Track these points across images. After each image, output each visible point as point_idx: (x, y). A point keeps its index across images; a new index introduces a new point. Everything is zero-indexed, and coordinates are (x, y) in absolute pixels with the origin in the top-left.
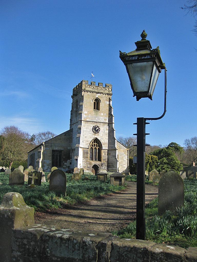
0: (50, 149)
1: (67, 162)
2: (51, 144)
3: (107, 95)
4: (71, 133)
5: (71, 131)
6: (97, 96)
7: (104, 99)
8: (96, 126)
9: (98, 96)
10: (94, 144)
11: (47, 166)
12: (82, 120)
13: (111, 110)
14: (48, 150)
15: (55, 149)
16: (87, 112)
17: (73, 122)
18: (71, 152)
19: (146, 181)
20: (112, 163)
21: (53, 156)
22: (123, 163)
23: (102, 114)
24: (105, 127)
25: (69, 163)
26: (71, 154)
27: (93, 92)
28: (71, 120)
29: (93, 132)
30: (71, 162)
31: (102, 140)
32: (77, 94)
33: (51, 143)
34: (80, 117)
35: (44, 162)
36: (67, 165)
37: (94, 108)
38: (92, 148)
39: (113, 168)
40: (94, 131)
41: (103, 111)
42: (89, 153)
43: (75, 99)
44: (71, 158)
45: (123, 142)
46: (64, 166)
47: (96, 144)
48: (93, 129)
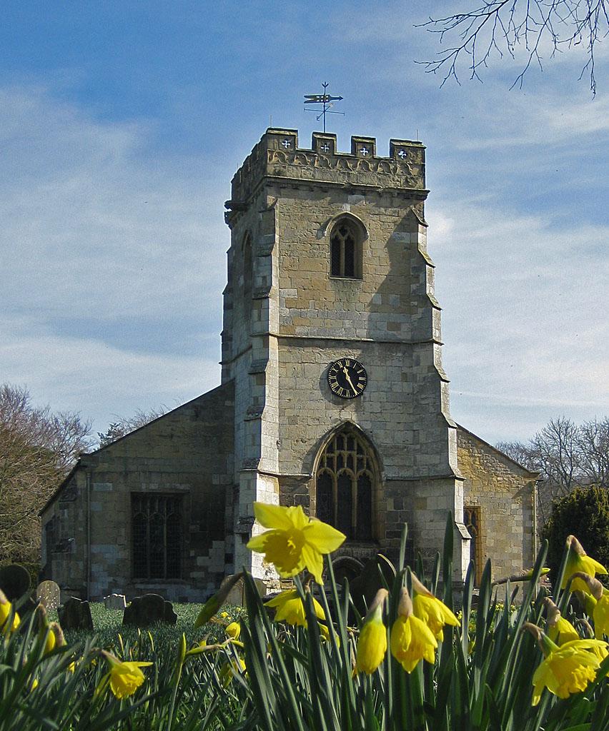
0: (122, 488)
1: (211, 551)
4: (228, 403)
5: (226, 392)
7: (384, 218)
8: (362, 382)
10: (340, 457)
11: (109, 576)
12: (271, 331)
13: (422, 275)
14: (109, 492)
16: (294, 291)
21: (137, 524)
22: (508, 550)
24: (396, 363)
26: (228, 511)
29: (333, 393)
30: (229, 552)
31: (381, 433)
32: (248, 205)
34: (260, 320)
35: (93, 554)
36: (210, 570)
37: (335, 271)
40: (337, 389)
41: (389, 386)
43: (242, 230)
45: (509, 451)
46: (195, 574)
47: (346, 453)
48: (331, 377)
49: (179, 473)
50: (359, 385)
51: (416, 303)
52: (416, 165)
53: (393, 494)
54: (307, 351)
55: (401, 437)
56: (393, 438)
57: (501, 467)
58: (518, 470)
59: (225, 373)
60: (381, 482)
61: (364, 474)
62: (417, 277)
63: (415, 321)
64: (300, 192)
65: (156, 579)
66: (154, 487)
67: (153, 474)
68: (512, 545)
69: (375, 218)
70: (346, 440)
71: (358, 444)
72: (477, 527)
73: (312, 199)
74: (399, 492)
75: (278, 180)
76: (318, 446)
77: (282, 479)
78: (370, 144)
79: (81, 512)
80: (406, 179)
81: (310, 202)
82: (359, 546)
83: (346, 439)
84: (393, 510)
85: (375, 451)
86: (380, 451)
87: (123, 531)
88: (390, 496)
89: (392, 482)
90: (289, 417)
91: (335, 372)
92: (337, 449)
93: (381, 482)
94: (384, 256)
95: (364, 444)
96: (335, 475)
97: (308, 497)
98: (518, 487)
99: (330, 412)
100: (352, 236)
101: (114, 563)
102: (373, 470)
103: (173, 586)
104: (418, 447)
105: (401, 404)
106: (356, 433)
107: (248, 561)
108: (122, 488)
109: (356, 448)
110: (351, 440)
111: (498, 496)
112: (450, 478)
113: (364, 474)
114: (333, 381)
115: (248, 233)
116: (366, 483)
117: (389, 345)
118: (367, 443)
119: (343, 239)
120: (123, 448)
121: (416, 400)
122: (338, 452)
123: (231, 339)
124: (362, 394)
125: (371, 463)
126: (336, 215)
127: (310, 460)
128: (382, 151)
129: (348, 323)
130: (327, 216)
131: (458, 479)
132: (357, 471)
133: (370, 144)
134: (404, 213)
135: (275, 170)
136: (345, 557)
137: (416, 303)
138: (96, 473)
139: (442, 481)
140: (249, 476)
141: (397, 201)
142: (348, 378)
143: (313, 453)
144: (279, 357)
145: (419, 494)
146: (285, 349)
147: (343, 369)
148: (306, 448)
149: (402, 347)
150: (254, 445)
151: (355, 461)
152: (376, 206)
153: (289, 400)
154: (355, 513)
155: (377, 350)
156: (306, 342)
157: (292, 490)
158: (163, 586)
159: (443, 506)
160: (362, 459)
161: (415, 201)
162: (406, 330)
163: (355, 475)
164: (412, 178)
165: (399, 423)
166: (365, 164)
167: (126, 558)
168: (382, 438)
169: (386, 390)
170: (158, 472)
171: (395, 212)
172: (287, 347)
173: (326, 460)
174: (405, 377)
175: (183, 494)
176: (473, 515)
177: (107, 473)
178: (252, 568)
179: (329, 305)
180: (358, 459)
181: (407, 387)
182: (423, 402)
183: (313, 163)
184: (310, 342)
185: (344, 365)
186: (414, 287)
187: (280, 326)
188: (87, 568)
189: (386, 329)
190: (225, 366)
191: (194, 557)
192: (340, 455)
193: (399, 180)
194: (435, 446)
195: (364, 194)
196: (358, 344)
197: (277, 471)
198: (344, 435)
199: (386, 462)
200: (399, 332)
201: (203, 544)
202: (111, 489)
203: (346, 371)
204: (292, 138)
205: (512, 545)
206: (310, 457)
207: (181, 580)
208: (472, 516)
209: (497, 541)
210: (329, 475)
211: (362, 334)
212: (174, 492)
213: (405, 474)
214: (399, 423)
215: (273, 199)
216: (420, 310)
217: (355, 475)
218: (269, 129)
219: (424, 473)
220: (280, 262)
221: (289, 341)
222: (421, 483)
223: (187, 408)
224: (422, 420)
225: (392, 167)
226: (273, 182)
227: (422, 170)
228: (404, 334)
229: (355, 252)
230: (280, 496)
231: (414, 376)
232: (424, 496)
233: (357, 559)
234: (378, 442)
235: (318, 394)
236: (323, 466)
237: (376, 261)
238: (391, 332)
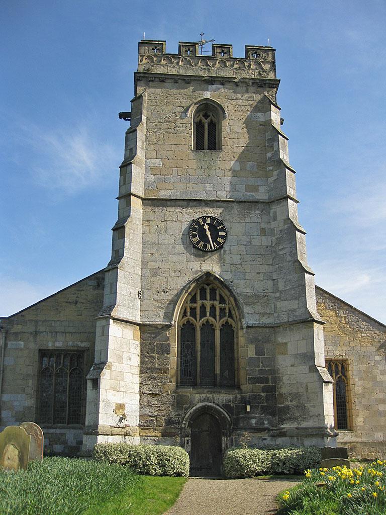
0: (32, 345)
2: (36, 326)
7: (240, 102)
8: (222, 237)
10: (203, 307)
12: (132, 191)
13: (275, 144)
14: (21, 349)
15: (50, 345)
19: (147, 90)
20: (297, 396)
21: (43, 373)
22: (375, 396)
24: (254, 219)
25: (121, 402)
29: (195, 247)
31: (241, 283)
33: (36, 322)
37: (199, 146)
39: (304, 419)
40: (198, 243)
47: (208, 303)
49: (80, 333)
50: (219, 239)
51: (271, 168)
52: (268, 62)
54: (170, 212)
55: (263, 286)
56: (253, 287)
57: (364, 325)
58: (379, 327)
61: (227, 322)
62: (272, 147)
63: (271, 183)
64: (165, 84)
65: (59, 425)
66: (59, 345)
68: (378, 392)
69: (232, 102)
70: (208, 291)
71: (220, 295)
72: (346, 377)
73: (177, 89)
74: (260, 338)
75: (146, 75)
76: (178, 296)
77: (143, 328)
78: (226, 49)
80: (259, 72)
81: (175, 91)
82: (220, 393)
83: (208, 289)
84: (255, 356)
85: (235, 300)
86: (240, 300)
87: (30, 382)
88: (252, 343)
89: (253, 330)
90: (151, 270)
91: (196, 227)
92: (200, 299)
94: (241, 131)
96: (198, 324)
97: (169, 345)
98: (380, 342)
99: (191, 265)
100: (214, 119)
101: (22, 410)
102: (235, 318)
103: (72, 430)
104: (278, 294)
105: (260, 256)
106: (217, 283)
107: (97, 408)
108: (32, 345)
109: (218, 298)
110: (213, 291)
111: (363, 349)
112: (308, 321)
113: (227, 322)
114: (194, 236)
116: (229, 332)
117: (248, 204)
118: (228, 293)
119: (206, 122)
120: (35, 313)
121: (275, 252)
122: (201, 302)
124: (222, 247)
125: (233, 312)
126: (198, 100)
127: (171, 309)
129: (208, 187)
130: (189, 102)
131: (316, 321)
132: (220, 319)
133: (226, 49)
134: (258, 97)
135: (144, 69)
136: (206, 403)
137: (271, 168)
138: (11, 333)
139: (301, 325)
140: (103, 322)
141: (252, 89)
142: (208, 233)
143: (174, 302)
144: (143, 216)
145: (280, 340)
146: (149, 209)
147: (204, 225)
148: (168, 298)
152: (234, 92)
153: (152, 254)
154: (217, 359)
155: (236, 208)
156: (169, 203)
157: (154, 338)
158: (63, 431)
159: (303, 350)
160: (225, 309)
161: (268, 89)
162: (263, 191)
163: (218, 324)
164: (264, 71)
166: (223, 62)
167: (32, 405)
168: (241, 287)
169: (245, 243)
170: (63, 332)
171: (250, 97)
172: (151, 208)
173: (188, 310)
174: (263, 232)
175: (84, 351)
176: (343, 367)
177: (20, 333)
178: (100, 415)
179: (191, 172)
180: (220, 309)
181: (265, 241)
182: (281, 253)
183: (178, 63)
184: (173, 203)
185: (205, 221)
186: (269, 155)
187: (145, 190)
189: (244, 191)
192: (203, 305)
193: (253, 73)
194: (293, 292)
195: (222, 84)
196: (218, 203)
197: (138, 320)
198: (206, 286)
199: (246, 310)
200: (256, 193)
202: (22, 347)
203: (206, 227)
205: (378, 392)
206: (171, 306)
207: (81, 425)
208: (338, 367)
209: (364, 388)
210: (192, 324)
211: (224, 195)
212: (75, 349)
213: (266, 320)
215: (142, 90)
216: (275, 173)
217: (218, 324)
219: (284, 318)
220: (146, 138)
221: (150, 202)
223: (91, 280)
224: (280, 269)
225: (246, 64)
226: (144, 77)
227: (273, 66)
228: (262, 195)
229: (217, 131)
230: (141, 344)
231: (272, 230)
232: (285, 341)
233: (218, 405)
234: (238, 291)
235: (180, 248)
236: (186, 316)
237: (234, 136)
238: (249, 194)
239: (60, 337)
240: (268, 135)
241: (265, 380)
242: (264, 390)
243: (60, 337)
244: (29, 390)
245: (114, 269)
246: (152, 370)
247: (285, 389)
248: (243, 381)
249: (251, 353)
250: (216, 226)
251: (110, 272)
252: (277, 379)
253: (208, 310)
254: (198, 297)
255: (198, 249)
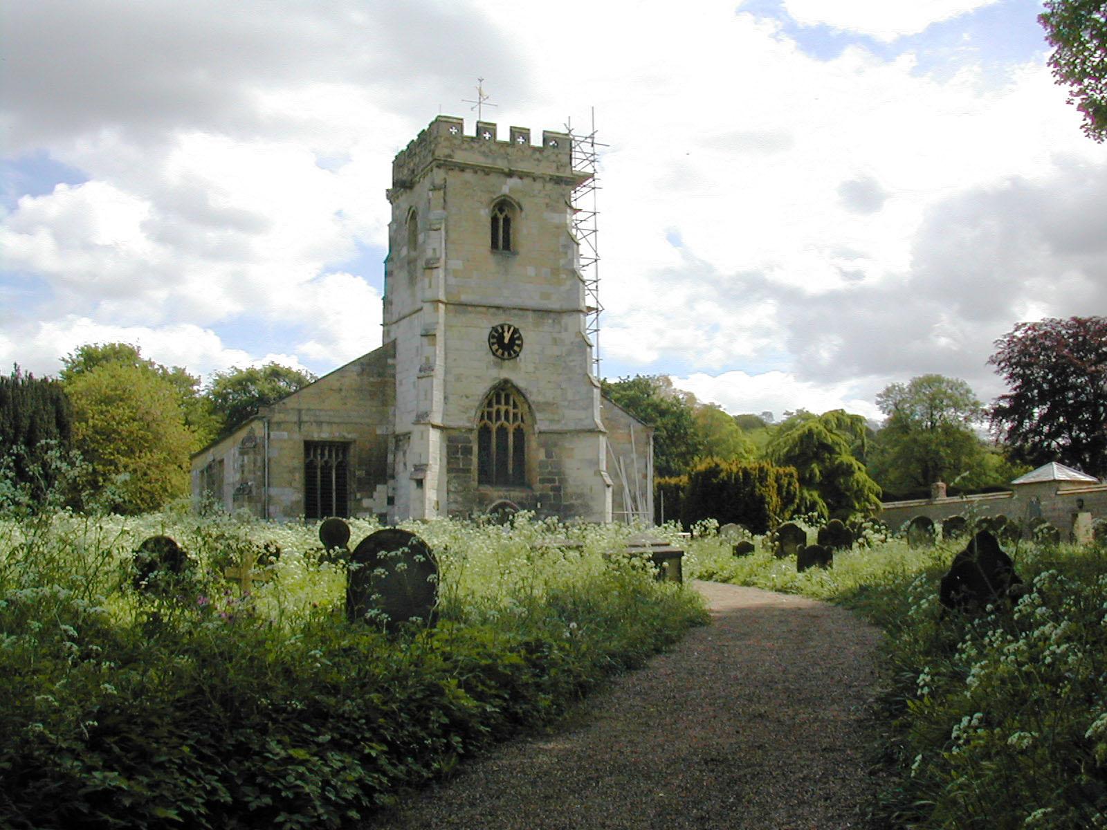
3: (549, 186)
4: (390, 361)
6: (505, 190)
9: (508, 187)
10: (498, 412)
14: (285, 441)
17: (396, 310)
18: (391, 446)
20: (580, 496)
21: (309, 468)
23: (531, 271)
27: (487, 171)
28: (387, 302)
29: (494, 354)
37: (494, 245)
38: (484, 432)
42: (475, 449)
44: (393, 477)
47: (503, 408)
48: (492, 341)
53: (544, 445)
59: (386, 334)
60: (534, 434)
61: (519, 426)
67: (324, 424)
70: (503, 396)
71: (514, 402)
78: (525, 133)
79: (259, 458)
85: (530, 407)
86: (533, 407)
87: (297, 476)
89: (544, 435)
93: (534, 434)
95: (519, 400)
96: (494, 427)
109: (512, 402)
110: (507, 397)
113: (519, 426)
114: (493, 344)
115: (412, 209)
116: (519, 434)
119: (501, 217)
123: (391, 303)
125: (525, 417)
128: (536, 141)
133: (525, 133)
139: (589, 434)
149: (552, 315)
150: (426, 399)
151: (511, 415)
154: (510, 462)
163: (511, 428)
165: (549, 382)
173: (486, 414)
177: (282, 422)
182: (572, 364)
188: (264, 509)
190: (386, 328)
191: (360, 500)
198: (501, 392)
199: (538, 416)
201: (368, 486)
204: (459, 124)
214: (549, 382)
217: (511, 428)
218: (439, 116)
219: (572, 426)
222: (569, 435)
239: (325, 427)
240: (563, 240)
241: (553, 481)
242: (552, 489)
243: (325, 427)
244: (295, 484)
245: (428, 376)
246: (458, 470)
247: (571, 487)
248: (288, 389)
249: (542, 455)
250: (516, 337)
251: (424, 379)
252: (562, 481)
253: (502, 413)
254: (494, 401)
255: (497, 356)
